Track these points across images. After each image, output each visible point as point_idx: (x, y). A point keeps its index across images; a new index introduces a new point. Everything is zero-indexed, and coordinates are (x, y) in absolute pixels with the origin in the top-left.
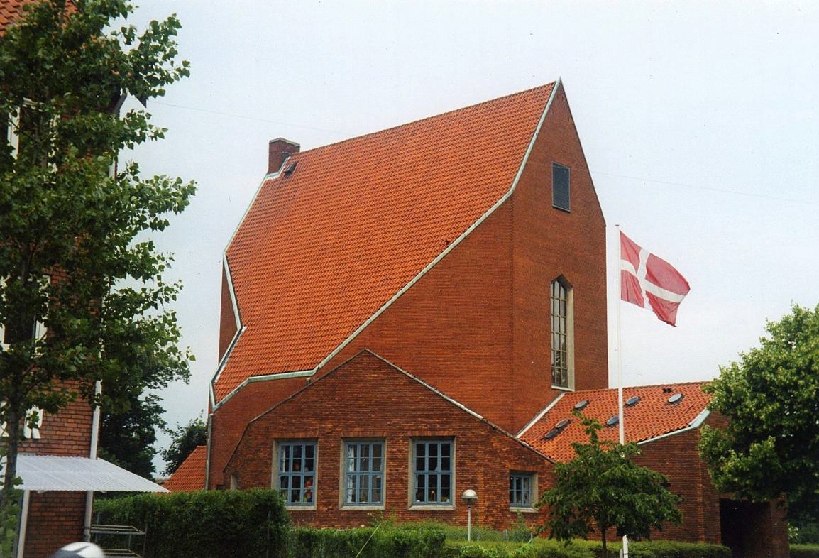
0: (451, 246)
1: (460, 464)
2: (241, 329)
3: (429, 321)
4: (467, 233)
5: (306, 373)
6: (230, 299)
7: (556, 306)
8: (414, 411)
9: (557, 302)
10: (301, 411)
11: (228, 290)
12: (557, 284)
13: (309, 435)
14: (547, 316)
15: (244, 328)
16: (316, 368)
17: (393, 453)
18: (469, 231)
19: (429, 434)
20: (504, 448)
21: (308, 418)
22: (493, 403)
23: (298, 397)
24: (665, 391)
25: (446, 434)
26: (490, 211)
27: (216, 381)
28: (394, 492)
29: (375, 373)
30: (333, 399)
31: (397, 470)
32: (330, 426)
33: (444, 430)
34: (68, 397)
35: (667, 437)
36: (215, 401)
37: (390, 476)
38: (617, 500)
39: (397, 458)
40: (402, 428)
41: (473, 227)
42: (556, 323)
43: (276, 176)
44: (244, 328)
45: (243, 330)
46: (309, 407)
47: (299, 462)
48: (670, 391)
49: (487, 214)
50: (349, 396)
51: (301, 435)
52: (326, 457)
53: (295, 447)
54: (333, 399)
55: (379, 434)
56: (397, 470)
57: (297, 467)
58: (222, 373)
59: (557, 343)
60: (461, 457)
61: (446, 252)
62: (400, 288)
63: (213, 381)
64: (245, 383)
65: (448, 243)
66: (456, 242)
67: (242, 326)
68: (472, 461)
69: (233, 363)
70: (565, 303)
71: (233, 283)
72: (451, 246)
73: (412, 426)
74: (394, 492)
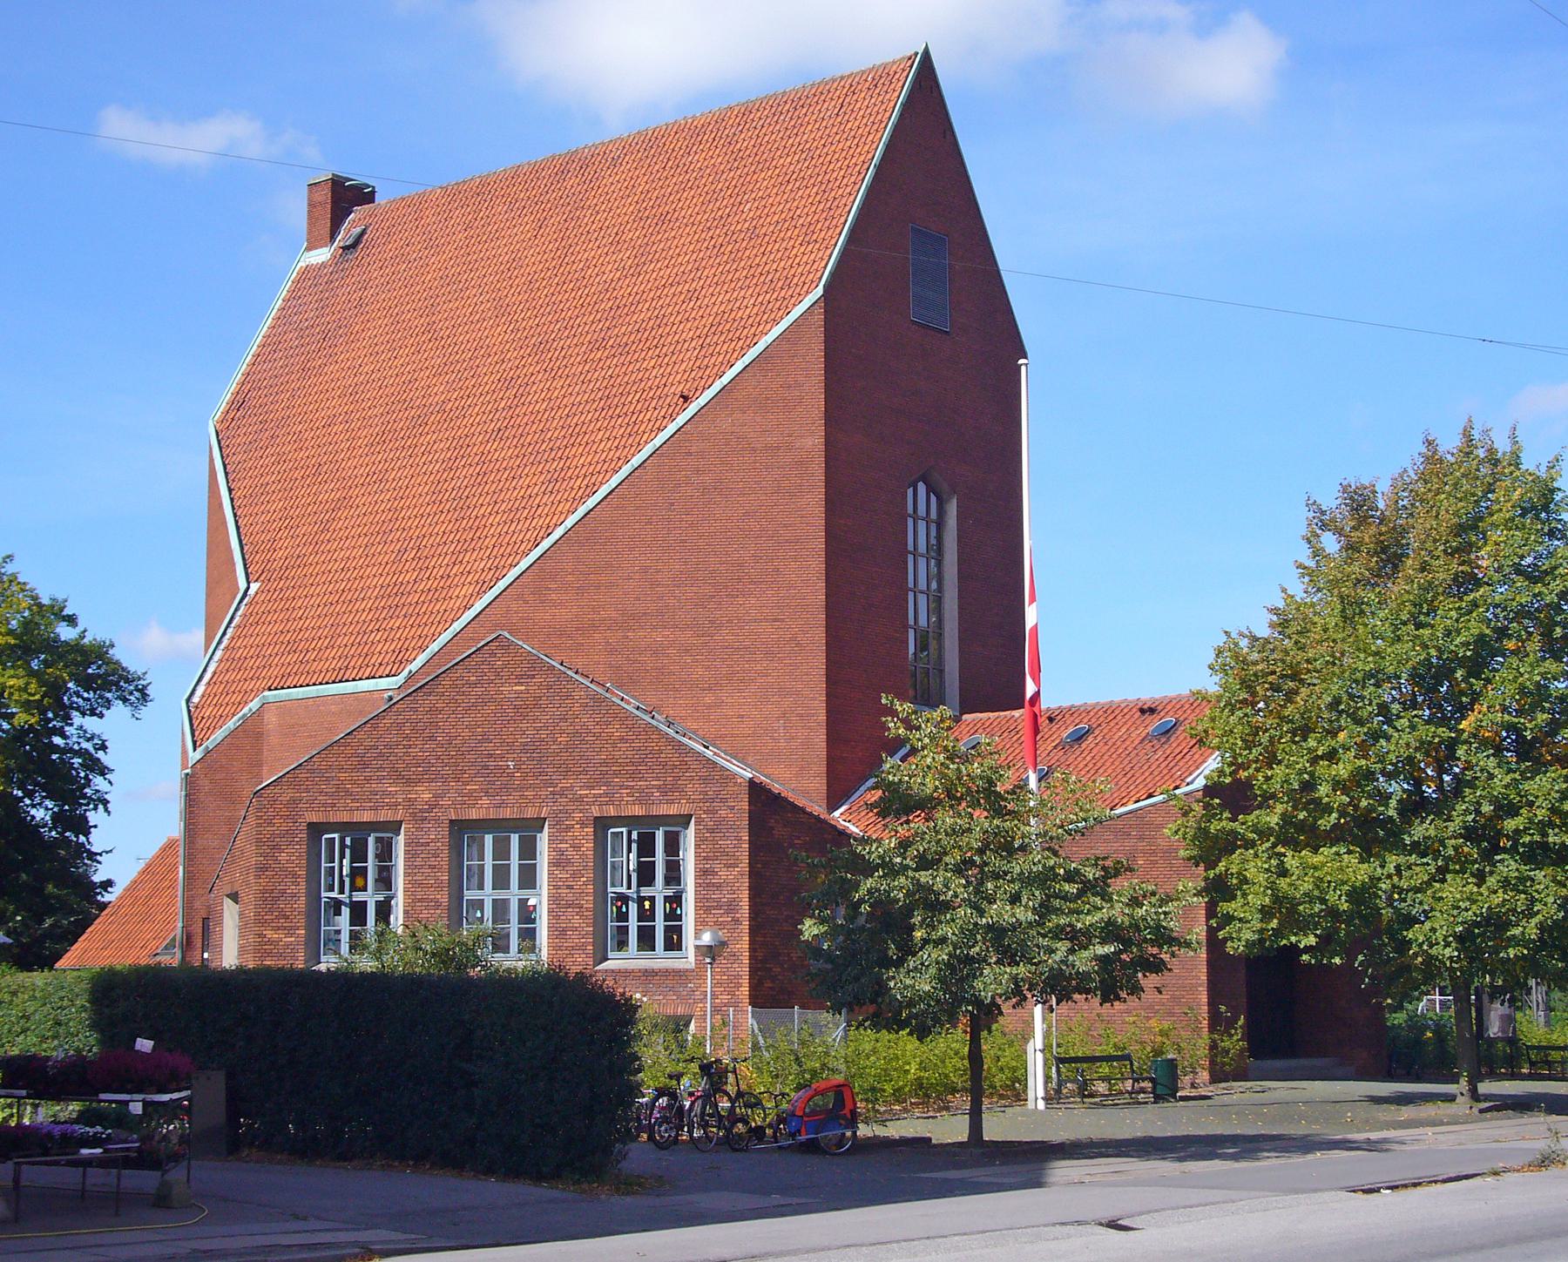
0: (693, 408)
1: (702, 873)
2: (248, 588)
3: (645, 570)
4: (725, 379)
5: (384, 683)
6: (224, 523)
7: (918, 535)
8: (604, 763)
9: (922, 526)
10: (366, 766)
11: (221, 505)
12: (921, 487)
13: (384, 816)
14: (899, 554)
15: (254, 587)
16: (406, 672)
17: (562, 852)
18: (731, 374)
19: (638, 811)
20: (799, 838)
21: (380, 779)
22: (783, 744)
23: (360, 735)
24: (1142, 711)
25: (673, 810)
26: (777, 331)
27: (196, 699)
28: (564, 931)
29: (521, 684)
30: (432, 738)
31: (569, 887)
32: (427, 796)
33: (672, 802)
34: (467, 931)
35: (1141, 809)
36: (194, 743)
37: (554, 899)
38: (992, 947)
39: (569, 862)
40: (581, 799)
41: (739, 366)
42: (919, 572)
43: (322, 255)
44: (254, 587)
45: (252, 592)
46: (381, 755)
47: (624, 931)
48: (1152, 711)
49: (769, 338)
50: (466, 733)
51: (366, 817)
52: (419, 862)
53: (378, 840)
54: (432, 738)
55: (530, 813)
56: (569, 887)
57: (359, 882)
58: (227, 648)
59: (919, 612)
60: (705, 858)
61: (682, 419)
62: (582, 500)
63: (188, 700)
64: (254, 705)
65: (686, 398)
66: (703, 400)
67: (249, 583)
68: (728, 866)
69: (232, 661)
70: (940, 525)
71: (230, 490)
72: (693, 408)
73: (600, 796)
74: (564, 931)
